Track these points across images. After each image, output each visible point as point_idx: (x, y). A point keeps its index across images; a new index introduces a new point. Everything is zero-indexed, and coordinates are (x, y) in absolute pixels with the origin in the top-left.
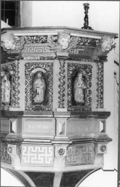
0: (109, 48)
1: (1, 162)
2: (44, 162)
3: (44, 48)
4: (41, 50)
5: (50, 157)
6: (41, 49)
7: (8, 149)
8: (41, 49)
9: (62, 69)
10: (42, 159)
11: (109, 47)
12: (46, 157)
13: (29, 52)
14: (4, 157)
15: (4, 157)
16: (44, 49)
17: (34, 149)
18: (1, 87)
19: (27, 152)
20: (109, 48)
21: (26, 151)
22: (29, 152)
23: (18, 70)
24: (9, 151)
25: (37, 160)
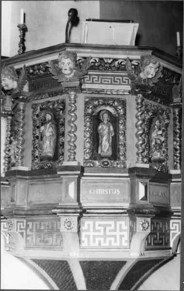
0: (152, 75)
1: (3, 76)
2: (94, 224)
3: (114, 78)
4: (110, 80)
5: (86, 231)
6: (109, 79)
7: (149, 226)
8: (109, 79)
9: (72, 144)
10: (97, 228)
11: (151, 73)
12: (91, 230)
13: (91, 77)
14: (161, 226)
15: (161, 226)
16: (111, 81)
17: (110, 242)
18: (1, 85)
19: (121, 236)
20: (152, 75)
21: (123, 238)
22: (118, 238)
23: (75, 143)
24: (148, 223)
25: (105, 227)
